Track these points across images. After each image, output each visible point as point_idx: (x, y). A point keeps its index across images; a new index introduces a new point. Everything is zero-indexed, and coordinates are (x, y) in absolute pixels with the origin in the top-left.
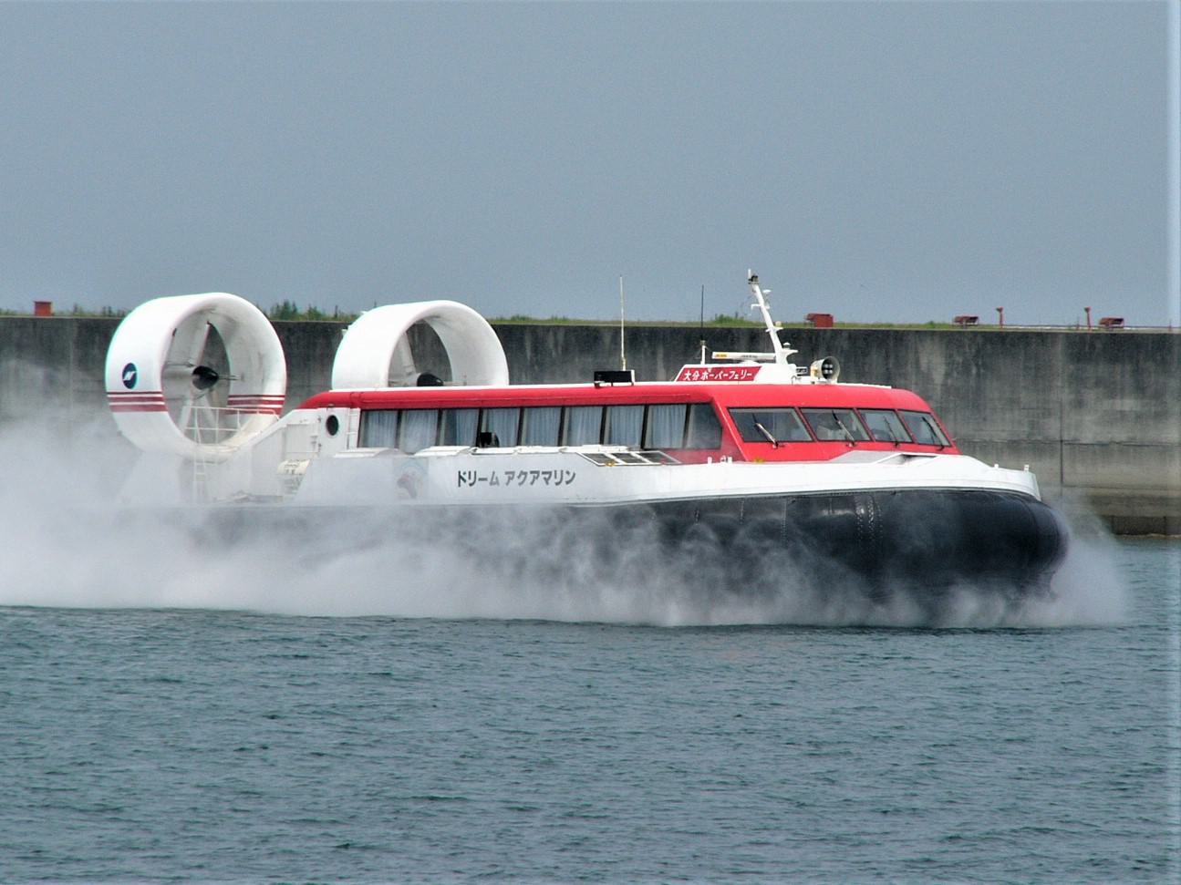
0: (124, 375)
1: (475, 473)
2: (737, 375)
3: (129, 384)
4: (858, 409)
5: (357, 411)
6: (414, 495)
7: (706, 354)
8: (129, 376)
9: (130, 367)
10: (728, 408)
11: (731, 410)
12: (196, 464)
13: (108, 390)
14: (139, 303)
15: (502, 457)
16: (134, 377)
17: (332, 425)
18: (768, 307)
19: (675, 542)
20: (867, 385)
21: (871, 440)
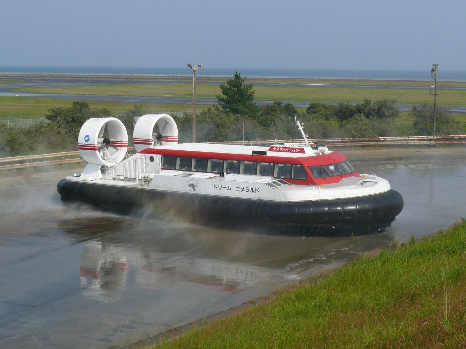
0: (85, 139)
1: (246, 188)
2: (294, 151)
3: (87, 141)
4: (326, 165)
5: (251, 154)
6: (194, 190)
7: (61, 152)
8: (87, 138)
9: (87, 136)
10: (308, 166)
11: (309, 167)
12: (106, 167)
13: (79, 143)
14: (89, 118)
15: (229, 177)
16: (89, 139)
17: (152, 159)
18: (299, 129)
19: (30, 129)
20: (256, 155)
21: (333, 176)
